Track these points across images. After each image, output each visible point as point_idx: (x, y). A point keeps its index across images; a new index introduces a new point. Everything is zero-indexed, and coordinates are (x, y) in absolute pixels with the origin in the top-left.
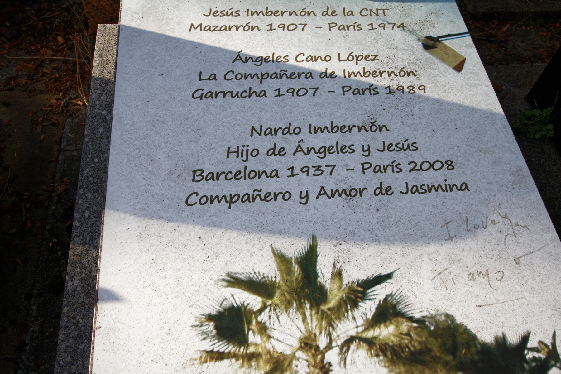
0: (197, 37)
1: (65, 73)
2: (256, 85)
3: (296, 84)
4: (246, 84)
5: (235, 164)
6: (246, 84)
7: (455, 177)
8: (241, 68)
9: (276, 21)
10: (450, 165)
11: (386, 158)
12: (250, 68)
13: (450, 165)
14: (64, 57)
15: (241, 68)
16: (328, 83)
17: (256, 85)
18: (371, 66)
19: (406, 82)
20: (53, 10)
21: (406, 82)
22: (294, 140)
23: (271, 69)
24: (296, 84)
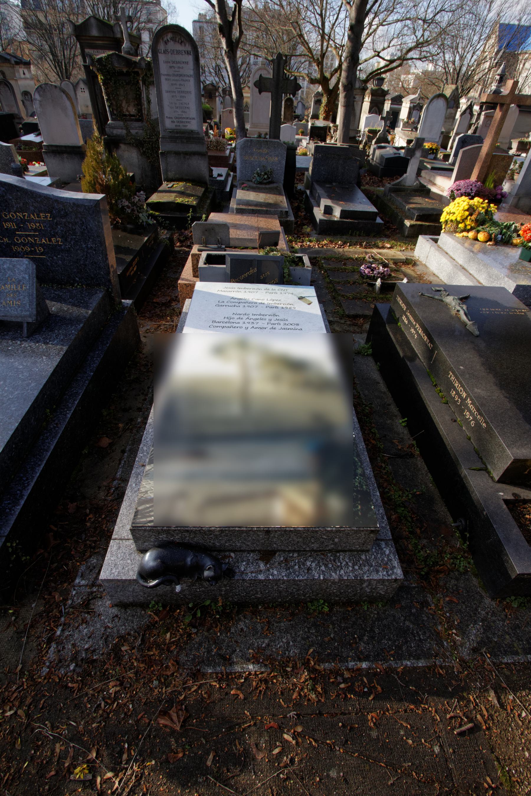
0: (220, 293)
1: (355, 529)
2: (237, 304)
3: (250, 305)
4: (234, 304)
5: (226, 320)
6: (234, 304)
7: (299, 327)
8: (233, 300)
9: (247, 290)
10: (298, 325)
11: (277, 322)
12: (236, 300)
13: (298, 325)
14: (397, 341)
15: (233, 300)
16: (262, 305)
17: (237, 304)
18: (278, 302)
19: (289, 306)
20: (124, 768)
21: (291, 306)
22: (247, 317)
23: (243, 301)
24: (250, 305)
